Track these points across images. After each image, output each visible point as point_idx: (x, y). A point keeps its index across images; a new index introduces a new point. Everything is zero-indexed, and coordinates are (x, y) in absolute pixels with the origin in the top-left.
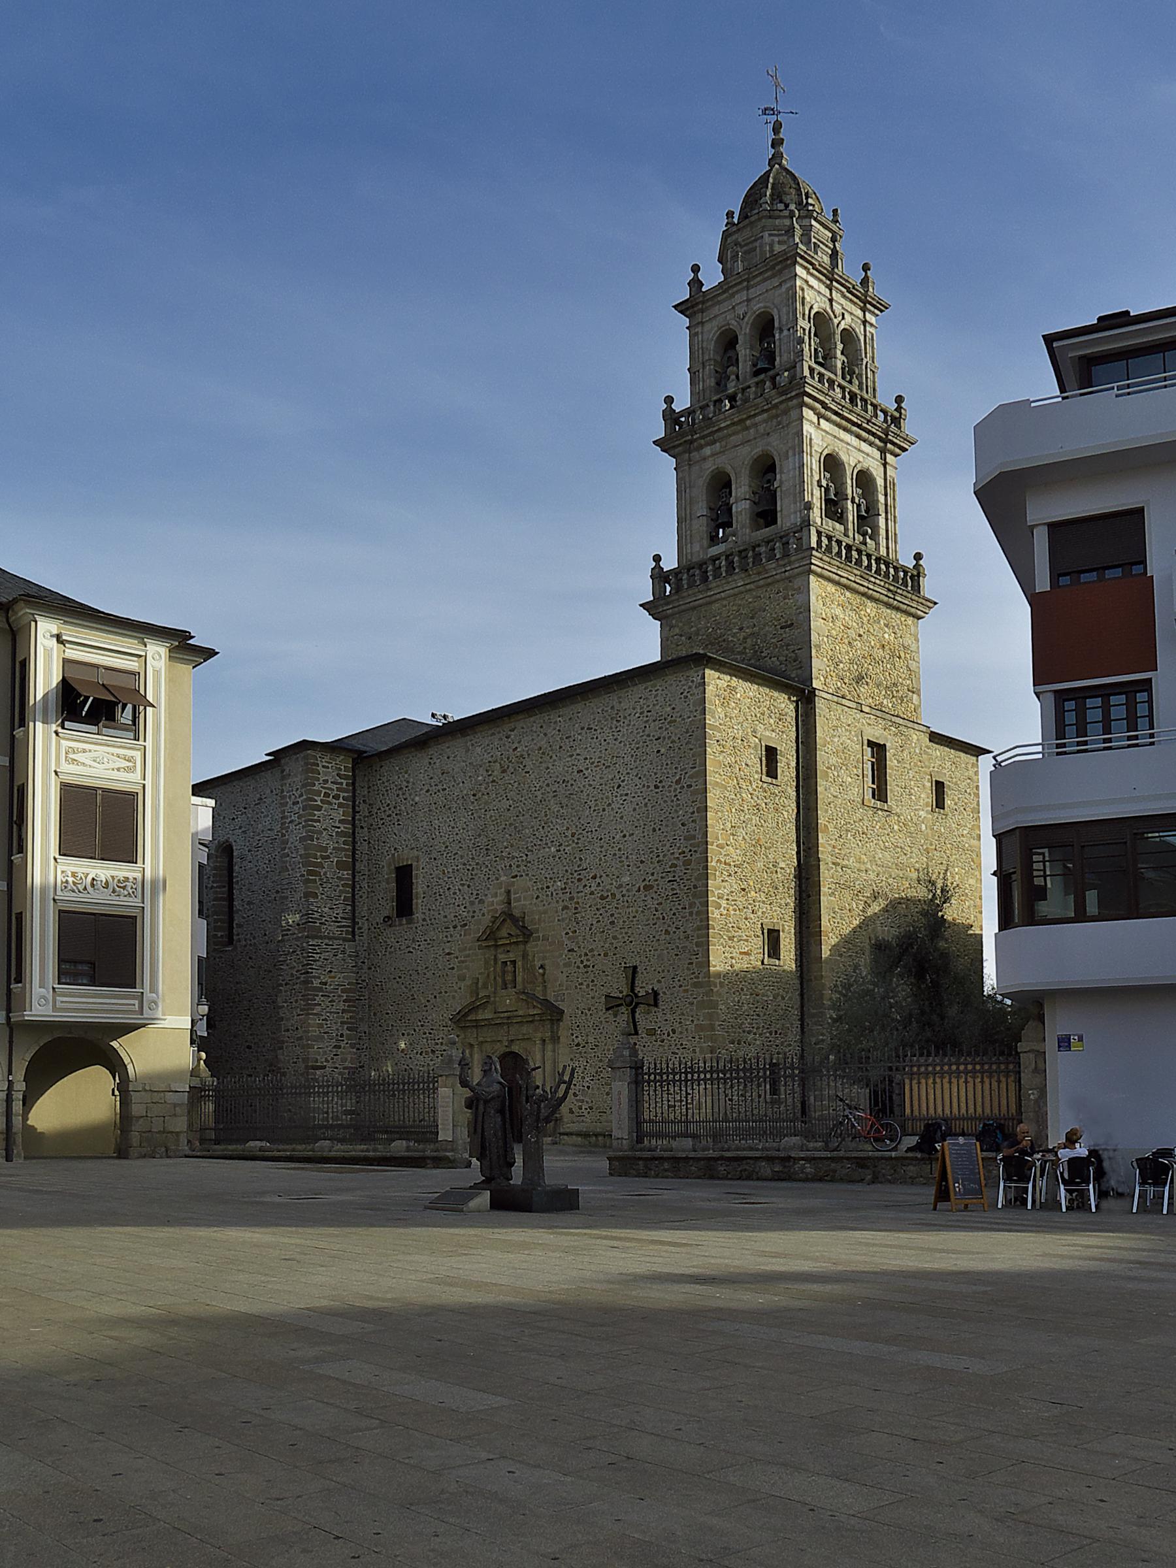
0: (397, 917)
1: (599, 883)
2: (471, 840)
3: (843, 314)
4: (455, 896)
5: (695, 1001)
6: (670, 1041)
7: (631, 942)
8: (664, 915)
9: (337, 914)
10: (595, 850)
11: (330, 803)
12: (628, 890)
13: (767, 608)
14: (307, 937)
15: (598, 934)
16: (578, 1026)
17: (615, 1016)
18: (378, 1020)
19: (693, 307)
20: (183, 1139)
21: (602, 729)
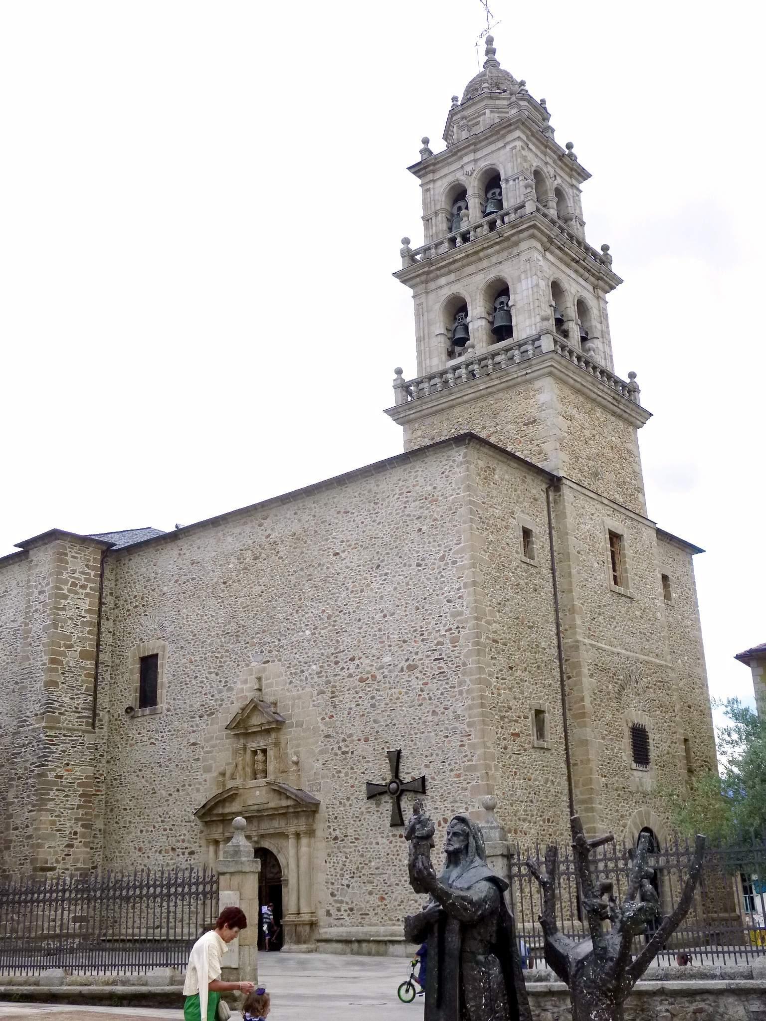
2: (220, 627)
5: (469, 786)
6: (440, 831)
7: (394, 725)
9: (78, 704)
11: (77, 593)
12: (390, 671)
14: (44, 727)
15: (357, 719)
16: (336, 818)
17: (378, 805)
18: (115, 816)
19: (425, 168)
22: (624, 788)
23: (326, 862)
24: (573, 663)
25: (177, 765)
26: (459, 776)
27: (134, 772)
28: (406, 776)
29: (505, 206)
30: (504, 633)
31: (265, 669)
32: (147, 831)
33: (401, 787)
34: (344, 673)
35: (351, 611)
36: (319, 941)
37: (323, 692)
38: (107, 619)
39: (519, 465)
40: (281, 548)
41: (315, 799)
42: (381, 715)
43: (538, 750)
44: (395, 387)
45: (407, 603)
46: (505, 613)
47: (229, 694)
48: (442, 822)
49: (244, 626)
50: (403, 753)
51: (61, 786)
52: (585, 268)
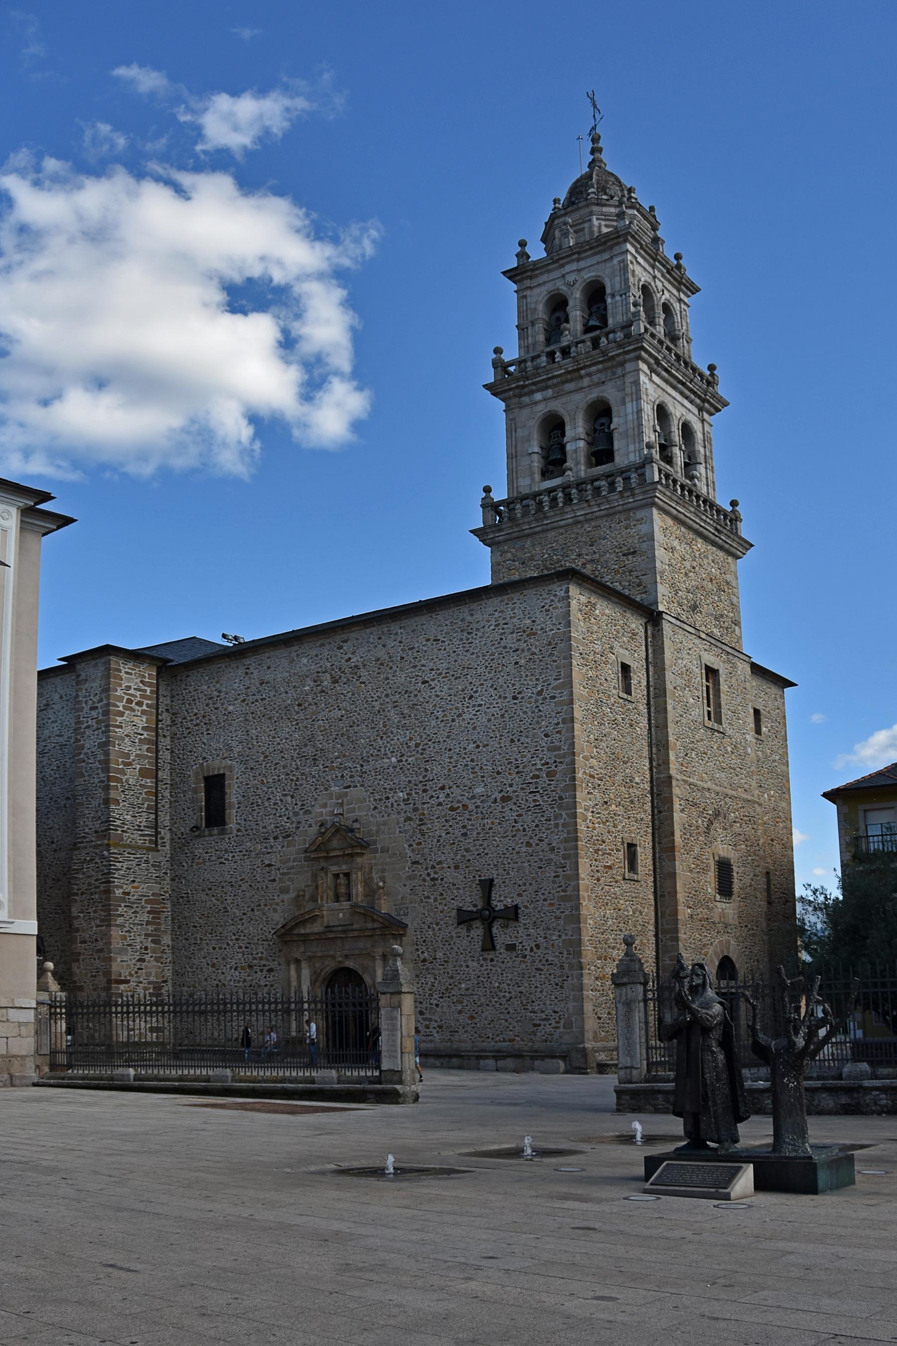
0: (206, 827)
1: (448, 794)
3: (663, 291)
4: (276, 807)
5: (563, 915)
6: (532, 956)
7: (487, 854)
8: (525, 826)
9: (140, 822)
10: (443, 760)
12: (482, 801)
13: (608, 536)
17: (468, 930)
18: (183, 933)
19: (522, 273)
20: (30, 1064)
21: (451, 640)
25: (251, 886)
26: (551, 905)
27: (203, 890)
28: (499, 904)
29: (610, 321)
31: (346, 794)
32: (220, 948)
34: (434, 801)
35: (441, 740)
38: (164, 736)
40: (363, 672)
44: (483, 506)
45: (501, 736)
47: (307, 817)
48: (534, 948)
49: (322, 750)
51: (129, 902)
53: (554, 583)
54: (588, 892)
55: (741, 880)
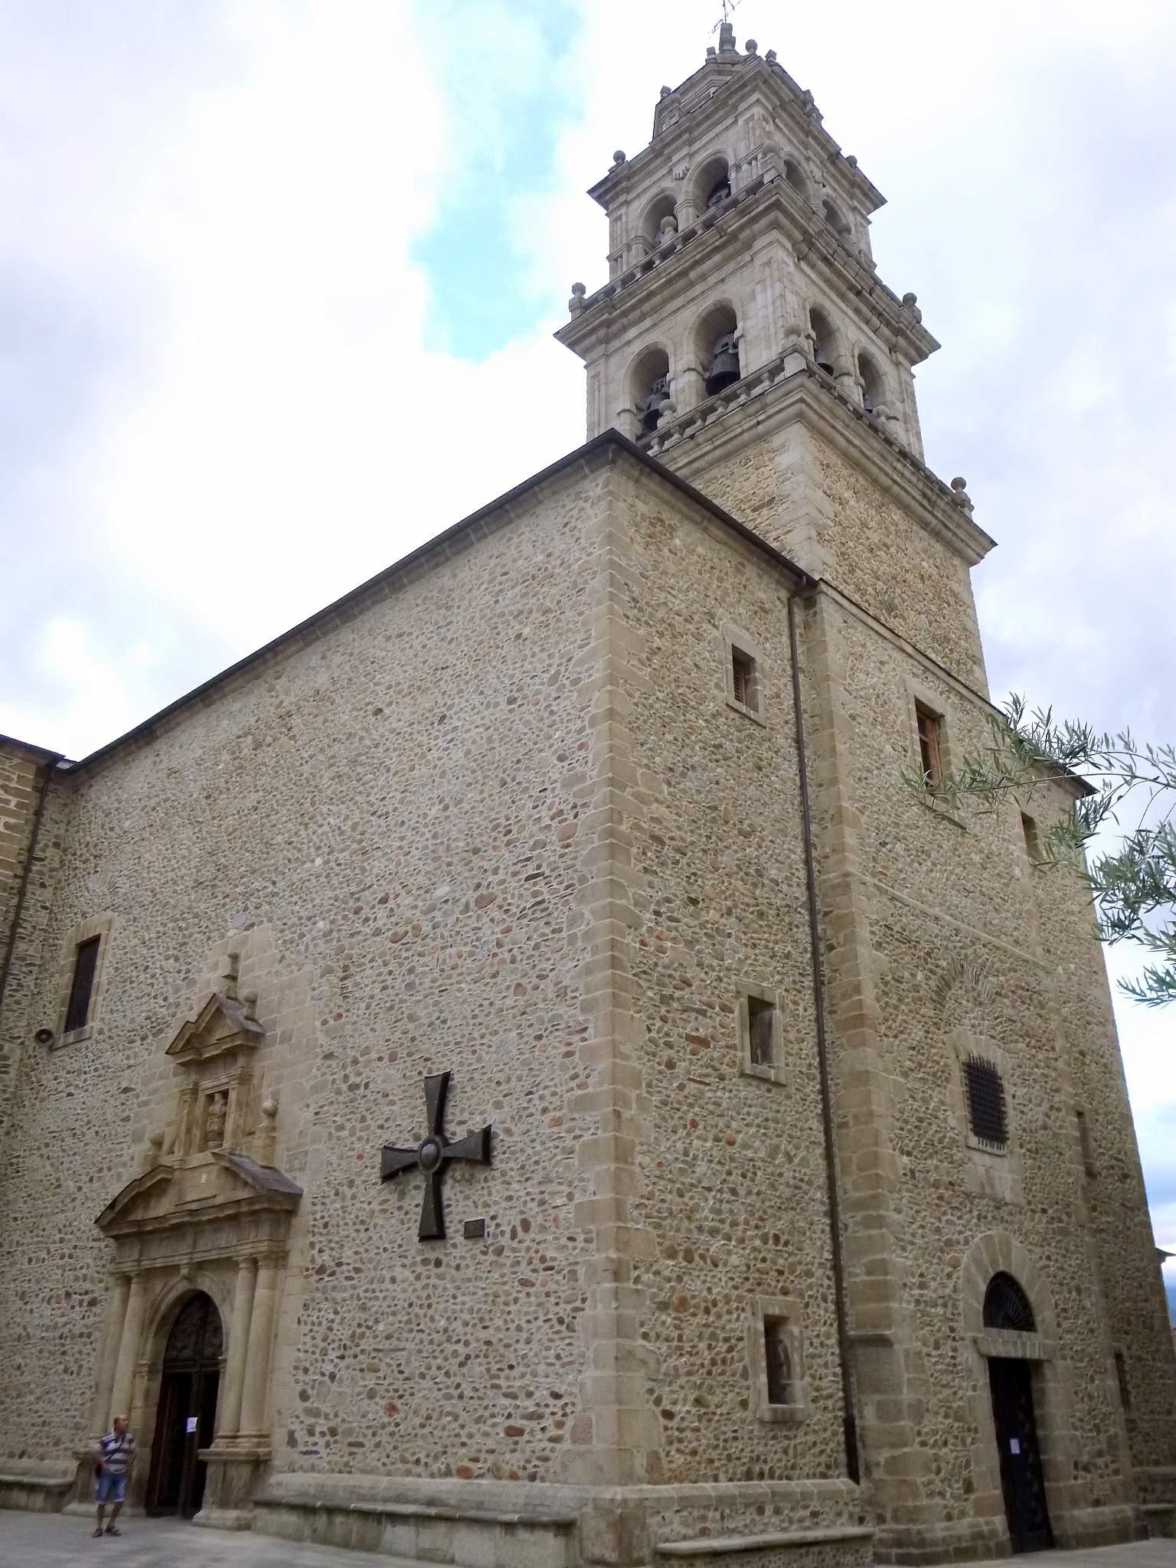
5: (577, 1145)
6: (514, 1250)
12: (446, 914)
16: (326, 1225)
17: (402, 1195)
19: (615, 186)
22: (951, 1183)
23: (299, 1322)
24: (838, 917)
26: (558, 1122)
30: (679, 828)
33: (446, 1152)
36: (258, 1504)
37: (329, 971)
39: (729, 535)
41: (291, 1185)
42: (422, 1005)
43: (754, 1083)
46: (684, 791)
48: (519, 1229)
50: (457, 1079)
52: (873, 309)
53: (584, 477)
54: (638, 1086)
55: (1022, 1112)
